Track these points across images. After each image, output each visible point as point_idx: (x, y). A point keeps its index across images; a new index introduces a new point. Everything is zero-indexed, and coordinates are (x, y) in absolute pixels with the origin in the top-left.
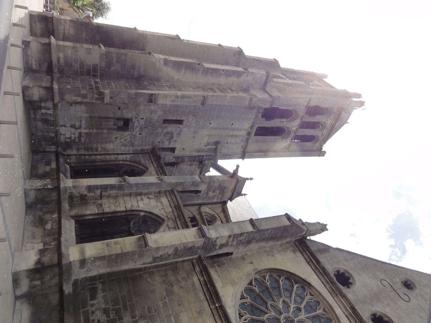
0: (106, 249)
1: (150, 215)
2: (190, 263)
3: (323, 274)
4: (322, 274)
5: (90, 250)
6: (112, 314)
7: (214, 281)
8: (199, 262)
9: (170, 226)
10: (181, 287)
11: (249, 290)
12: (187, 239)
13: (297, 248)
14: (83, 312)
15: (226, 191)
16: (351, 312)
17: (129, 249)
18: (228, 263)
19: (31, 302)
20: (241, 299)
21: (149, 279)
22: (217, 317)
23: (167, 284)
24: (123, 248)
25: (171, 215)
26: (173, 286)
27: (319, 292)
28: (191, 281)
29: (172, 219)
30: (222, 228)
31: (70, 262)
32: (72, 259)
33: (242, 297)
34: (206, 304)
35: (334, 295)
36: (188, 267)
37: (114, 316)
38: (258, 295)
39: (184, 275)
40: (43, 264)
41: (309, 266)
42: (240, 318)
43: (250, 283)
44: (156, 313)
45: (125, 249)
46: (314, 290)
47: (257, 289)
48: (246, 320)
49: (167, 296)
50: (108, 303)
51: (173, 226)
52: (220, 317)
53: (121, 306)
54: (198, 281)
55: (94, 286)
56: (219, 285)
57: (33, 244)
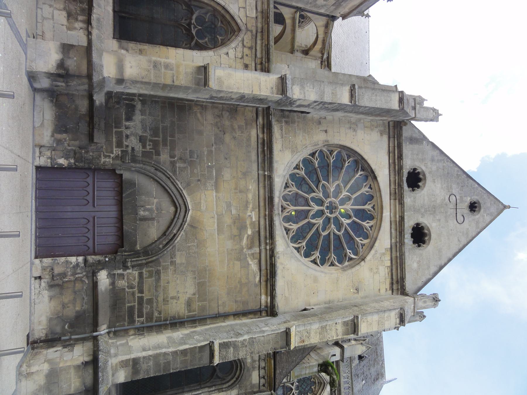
0: (152, 71)
1: (223, 12)
2: (255, 109)
3: (397, 173)
4: (395, 172)
5: (131, 67)
6: (149, 145)
7: (274, 140)
8: (265, 113)
9: (245, 43)
10: (234, 138)
11: (307, 162)
12: (260, 90)
13: (387, 130)
14: (116, 131)
15: (344, 5)
16: (398, 220)
17: (182, 83)
18: (298, 122)
19: (54, 101)
20: (294, 168)
21: (199, 115)
22: (261, 185)
23: (219, 128)
24: (175, 78)
25: (251, 25)
26: (224, 134)
27: (380, 189)
28: (248, 133)
29: (251, 31)
30: (311, 87)
31: (104, 78)
32: (106, 75)
33: (297, 167)
34: (255, 166)
35: (392, 198)
36: (251, 115)
37: (150, 149)
38: (315, 169)
39: (242, 123)
40: (67, 70)
41: (387, 157)
42: (285, 188)
43: (313, 154)
44: (198, 160)
45: (177, 80)
46: (376, 185)
47: (317, 163)
48: (290, 192)
49: (215, 143)
50: (146, 131)
51: (249, 45)
52: (265, 187)
53: (160, 139)
54: (256, 136)
55: (132, 103)
56: (277, 146)
57: (52, 9)
